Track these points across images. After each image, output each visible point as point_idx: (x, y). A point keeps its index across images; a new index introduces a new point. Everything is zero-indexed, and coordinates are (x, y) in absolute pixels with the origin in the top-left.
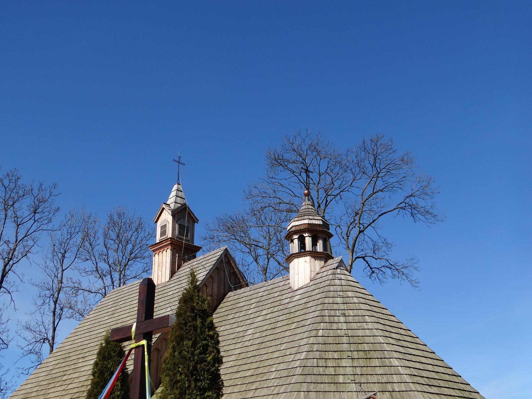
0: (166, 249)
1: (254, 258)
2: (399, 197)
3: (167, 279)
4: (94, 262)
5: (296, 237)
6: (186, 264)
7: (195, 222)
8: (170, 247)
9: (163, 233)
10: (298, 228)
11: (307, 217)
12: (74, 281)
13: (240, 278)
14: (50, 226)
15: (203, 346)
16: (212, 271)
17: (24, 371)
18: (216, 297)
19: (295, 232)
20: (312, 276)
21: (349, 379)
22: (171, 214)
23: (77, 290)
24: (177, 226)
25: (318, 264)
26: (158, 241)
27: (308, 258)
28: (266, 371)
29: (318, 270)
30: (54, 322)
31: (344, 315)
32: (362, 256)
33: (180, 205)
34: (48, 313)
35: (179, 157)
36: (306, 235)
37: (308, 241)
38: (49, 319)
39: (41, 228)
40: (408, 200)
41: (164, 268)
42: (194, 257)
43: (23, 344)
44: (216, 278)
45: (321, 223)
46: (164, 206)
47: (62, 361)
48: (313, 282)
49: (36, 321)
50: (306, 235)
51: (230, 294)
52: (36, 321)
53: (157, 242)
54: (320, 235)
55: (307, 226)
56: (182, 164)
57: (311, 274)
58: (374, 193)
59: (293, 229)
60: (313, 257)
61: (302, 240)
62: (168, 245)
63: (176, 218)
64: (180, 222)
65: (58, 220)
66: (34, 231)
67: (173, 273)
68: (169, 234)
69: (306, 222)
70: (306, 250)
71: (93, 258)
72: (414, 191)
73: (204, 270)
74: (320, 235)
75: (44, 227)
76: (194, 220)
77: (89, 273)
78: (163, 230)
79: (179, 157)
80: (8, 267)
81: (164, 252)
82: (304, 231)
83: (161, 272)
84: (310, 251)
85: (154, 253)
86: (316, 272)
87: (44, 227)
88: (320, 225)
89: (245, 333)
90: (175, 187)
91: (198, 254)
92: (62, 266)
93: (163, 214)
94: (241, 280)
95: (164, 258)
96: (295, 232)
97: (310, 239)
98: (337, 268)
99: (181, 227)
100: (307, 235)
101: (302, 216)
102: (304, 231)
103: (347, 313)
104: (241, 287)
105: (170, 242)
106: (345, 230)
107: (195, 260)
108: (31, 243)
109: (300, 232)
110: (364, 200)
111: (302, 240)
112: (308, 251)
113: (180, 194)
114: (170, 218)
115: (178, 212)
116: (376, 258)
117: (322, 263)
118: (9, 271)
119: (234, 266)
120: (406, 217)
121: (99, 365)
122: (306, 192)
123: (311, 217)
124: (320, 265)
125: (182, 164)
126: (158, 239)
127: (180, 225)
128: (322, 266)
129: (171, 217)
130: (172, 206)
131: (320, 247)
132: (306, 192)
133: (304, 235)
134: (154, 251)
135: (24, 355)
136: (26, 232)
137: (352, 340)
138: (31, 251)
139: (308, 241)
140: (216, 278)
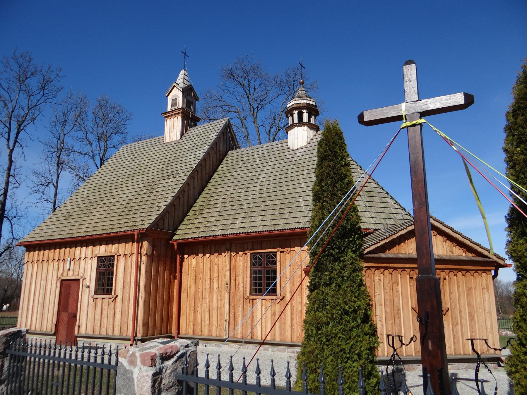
0: (177, 116)
3: (179, 138)
4: (85, 133)
5: (296, 112)
6: (191, 129)
7: (197, 100)
8: (181, 115)
9: (174, 103)
10: (297, 106)
11: (306, 98)
12: (69, 145)
13: (236, 142)
14: (55, 100)
17: (32, 205)
18: (221, 153)
19: (296, 108)
20: (308, 141)
21: (363, 209)
22: (182, 90)
23: (70, 151)
26: (169, 110)
27: (306, 128)
28: (293, 201)
29: (312, 137)
30: (58, 171)
34: (54, 164)
37: (305, 116)
38: (54, 169)
39: (47, 101)
41: (175, 130)
42: (196, 125)
43: (31, 185)
44: (222, 139)
46: (175, 84)
48: (309, 145)
49: (45, 169)
51: (230, 152)
52: (45, 169)
53: (168, 111)
55: (305, 105)
57: (307, 139)
59: (294, 106)
60: (309, 127)
61: (300, 115)
62: (179, 113)
63: (185, 95)
66: (42, 103)
67: (182, 134)
68: (180, 105)
69: (305, 101)
70: (304, 122)
71: (83, 129)
75: (51, 101)
76: (196, 99)
77: (80, 140)
78: (174, 102)
80: (22, 128)
81: (176, 118)
82: (303, 108)
83: (172, 133)
84: (306, 123)
85: (166, 119)
87: (51, 101)
89: (258, 177)
90: (182, 72)
91: (198, 123)
92: (63, 131)
93: (173, 90)
94: (236, 144)
95: (175, 123)
96: (296, 108)
100: (305, 111)
101: (301, 97)
102: (303, 108)
105: (181, 111)
106: (268, 128)
107: (196, 127)
108: (37, 112)
109: (300, 108)
110: (283, 110)
111: (300, 115)
112: (305, 123)
113: (186, 78)
114: (180, 94)
115: (186, 91)
118: (22, 130)
122: (301, 81)
123: (308, 99)
124: (313, 133)
126: (169, 108)
127: (187, 100)
128: (314, 135)
129: (181, 93)
130: (181, 85)
131: (312, 120)
132: (301, 81)
133: (303, 111)
134: (165, 117)
135: (31, 194)
136: (36, 102)
138: (36, 119)
139: (305, 116)
140: (222, 139)
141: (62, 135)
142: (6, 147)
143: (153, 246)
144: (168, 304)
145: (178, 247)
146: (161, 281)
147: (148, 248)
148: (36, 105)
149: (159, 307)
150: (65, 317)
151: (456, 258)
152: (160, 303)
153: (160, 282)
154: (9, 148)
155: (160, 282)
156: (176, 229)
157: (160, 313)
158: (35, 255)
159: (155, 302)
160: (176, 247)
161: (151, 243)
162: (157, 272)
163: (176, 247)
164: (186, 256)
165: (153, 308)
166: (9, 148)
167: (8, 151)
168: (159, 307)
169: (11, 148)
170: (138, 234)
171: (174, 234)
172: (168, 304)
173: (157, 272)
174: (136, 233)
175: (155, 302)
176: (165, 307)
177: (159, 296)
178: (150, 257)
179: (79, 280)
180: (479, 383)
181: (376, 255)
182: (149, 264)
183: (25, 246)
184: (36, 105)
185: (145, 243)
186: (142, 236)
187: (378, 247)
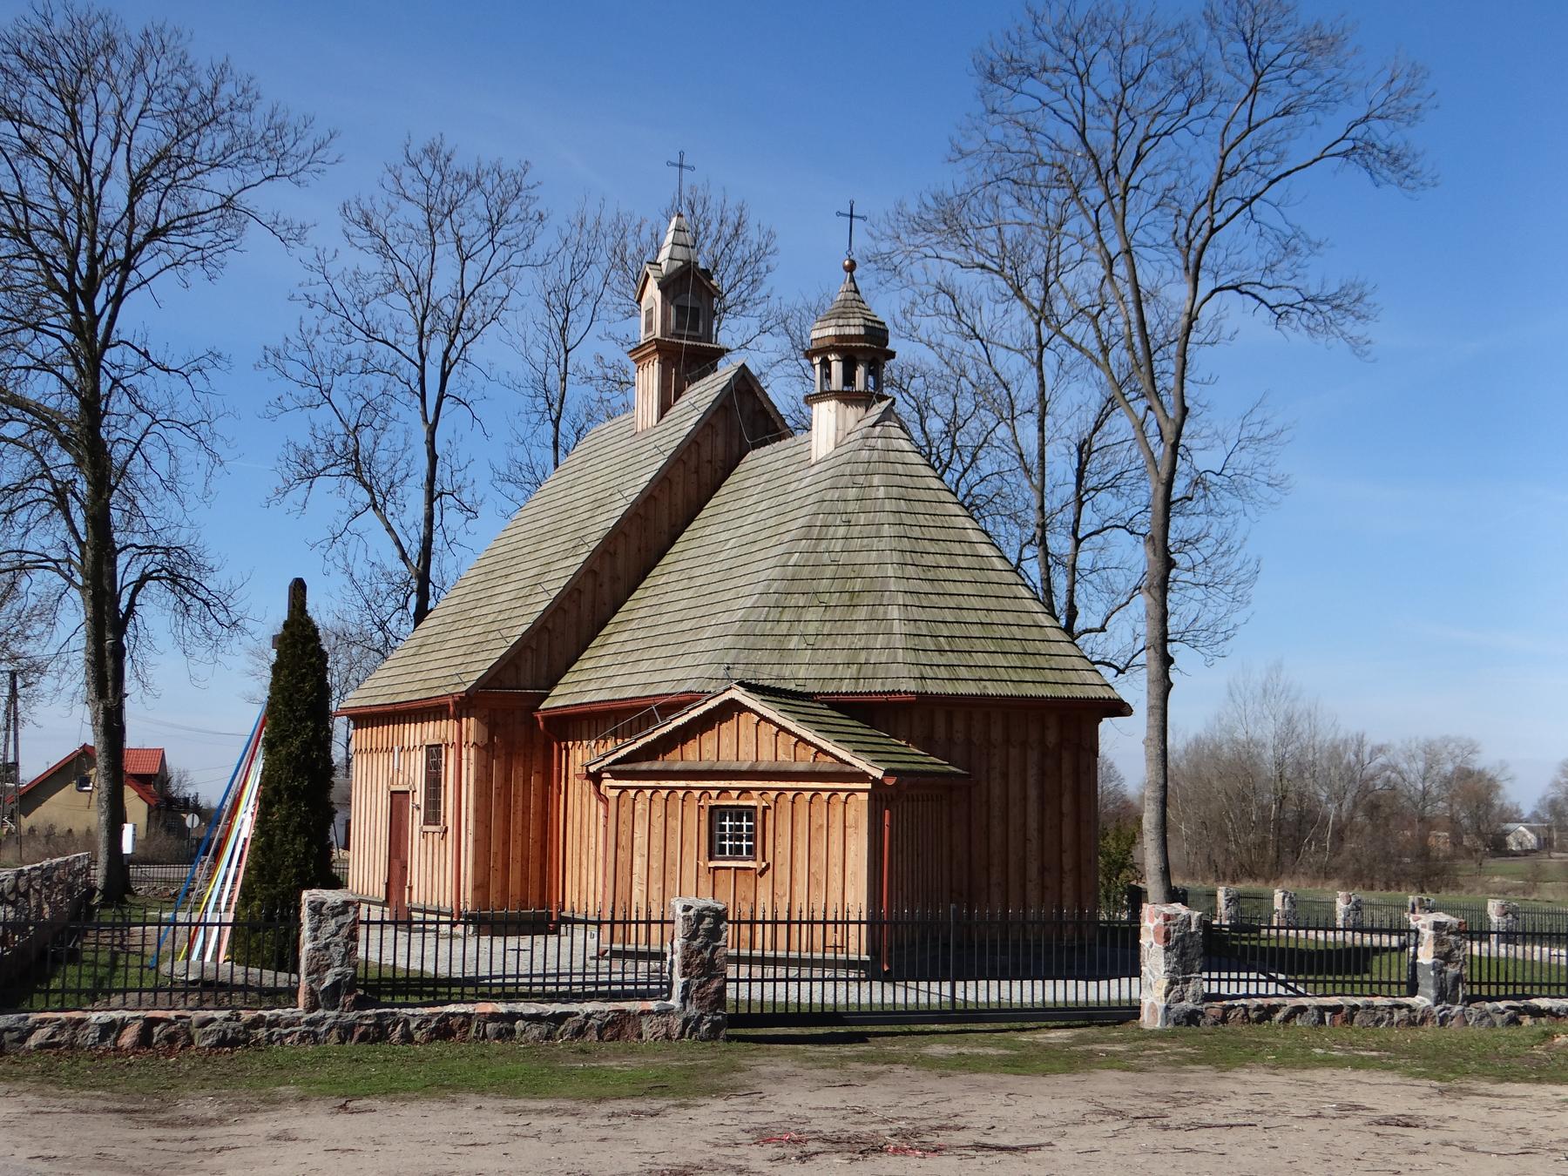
1: (404, 557)
2: (1333, 125)
6: (691, 388)
11: (833, 322)
15: (302, 675)
16: (710, 413)
24: (673, 311)
25: (853, 413)
27: (833, 404)
31: (848, 523)
32: (1230, 284)
33: (681, 263)
35: (681, 154)
36: (832, 357)
40: (1357, 131)
45: (862, 331)
47: (482, 578)
50: (832, 357)
54: (860, 357)
56: (688, 168)
57: (836, 435)
58: (1250, 130)
62: (654, 352)
64: (679, 301)
65: (546, 241)
67: (662, 415)
72: (1375, 106)
73: (696, 412)
74: (860, 357)
79: (681, 154)
86: (847, 431)
88: (860, 335)
97: (840, 365)
98: (874, 426)
99: (681, 310)
103: (854, 518)
104: (780, 438)
114: (658, 295)
116: (1270, 285)
117: (862, 410)
119: (762, 399)
120: (1353, 173)
121: (1003, 431)
124: (857, 415)
125: (688, 168)
137: (841, 572)
141: (563, 350)
142: (420, 417)
143: (492, 725)
144: (543, 847)
145: (545, 725)
146: (520, 799)
147: (477, 731)
148: (480, 284)
149: (515, 852)
150: (396, 863)
151: (782, 769)
152: (519, 843)
153: (516, 802)
154: (426, 420)
155: (516, 802)
156: (553, 684)
157: (519, 865)
158: (380, 735)
159: (506, 843)
160: (541, 724)
161: (486, 720)
162: (507, 779)
163: (541, 724)
164: (570, 744)
165: (500, 856)
166: (426, 420)
167: (424, 429)
168: (515, 852)
169: (431, 419)
170: (455, 703)
171: (546, 696)
172: (543, 847)
173: (507, 779)
174: (450, 701)
175: (506, 843)
176: (534, 852)
177: (515, 831)
178: (486, 751)
179: (407, 792)
180: (434, 926)
181: (644, 766)
182: (484, 763)
183: (351, 717)
184: (480, 284)
185: (472, 719)
186: (463, 706)
187: (633, 751)
